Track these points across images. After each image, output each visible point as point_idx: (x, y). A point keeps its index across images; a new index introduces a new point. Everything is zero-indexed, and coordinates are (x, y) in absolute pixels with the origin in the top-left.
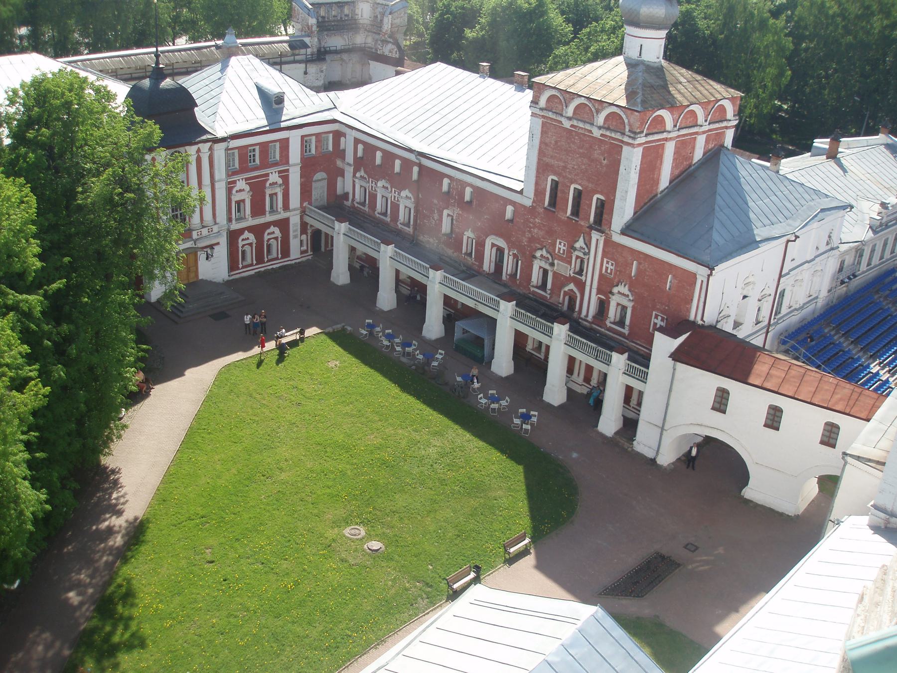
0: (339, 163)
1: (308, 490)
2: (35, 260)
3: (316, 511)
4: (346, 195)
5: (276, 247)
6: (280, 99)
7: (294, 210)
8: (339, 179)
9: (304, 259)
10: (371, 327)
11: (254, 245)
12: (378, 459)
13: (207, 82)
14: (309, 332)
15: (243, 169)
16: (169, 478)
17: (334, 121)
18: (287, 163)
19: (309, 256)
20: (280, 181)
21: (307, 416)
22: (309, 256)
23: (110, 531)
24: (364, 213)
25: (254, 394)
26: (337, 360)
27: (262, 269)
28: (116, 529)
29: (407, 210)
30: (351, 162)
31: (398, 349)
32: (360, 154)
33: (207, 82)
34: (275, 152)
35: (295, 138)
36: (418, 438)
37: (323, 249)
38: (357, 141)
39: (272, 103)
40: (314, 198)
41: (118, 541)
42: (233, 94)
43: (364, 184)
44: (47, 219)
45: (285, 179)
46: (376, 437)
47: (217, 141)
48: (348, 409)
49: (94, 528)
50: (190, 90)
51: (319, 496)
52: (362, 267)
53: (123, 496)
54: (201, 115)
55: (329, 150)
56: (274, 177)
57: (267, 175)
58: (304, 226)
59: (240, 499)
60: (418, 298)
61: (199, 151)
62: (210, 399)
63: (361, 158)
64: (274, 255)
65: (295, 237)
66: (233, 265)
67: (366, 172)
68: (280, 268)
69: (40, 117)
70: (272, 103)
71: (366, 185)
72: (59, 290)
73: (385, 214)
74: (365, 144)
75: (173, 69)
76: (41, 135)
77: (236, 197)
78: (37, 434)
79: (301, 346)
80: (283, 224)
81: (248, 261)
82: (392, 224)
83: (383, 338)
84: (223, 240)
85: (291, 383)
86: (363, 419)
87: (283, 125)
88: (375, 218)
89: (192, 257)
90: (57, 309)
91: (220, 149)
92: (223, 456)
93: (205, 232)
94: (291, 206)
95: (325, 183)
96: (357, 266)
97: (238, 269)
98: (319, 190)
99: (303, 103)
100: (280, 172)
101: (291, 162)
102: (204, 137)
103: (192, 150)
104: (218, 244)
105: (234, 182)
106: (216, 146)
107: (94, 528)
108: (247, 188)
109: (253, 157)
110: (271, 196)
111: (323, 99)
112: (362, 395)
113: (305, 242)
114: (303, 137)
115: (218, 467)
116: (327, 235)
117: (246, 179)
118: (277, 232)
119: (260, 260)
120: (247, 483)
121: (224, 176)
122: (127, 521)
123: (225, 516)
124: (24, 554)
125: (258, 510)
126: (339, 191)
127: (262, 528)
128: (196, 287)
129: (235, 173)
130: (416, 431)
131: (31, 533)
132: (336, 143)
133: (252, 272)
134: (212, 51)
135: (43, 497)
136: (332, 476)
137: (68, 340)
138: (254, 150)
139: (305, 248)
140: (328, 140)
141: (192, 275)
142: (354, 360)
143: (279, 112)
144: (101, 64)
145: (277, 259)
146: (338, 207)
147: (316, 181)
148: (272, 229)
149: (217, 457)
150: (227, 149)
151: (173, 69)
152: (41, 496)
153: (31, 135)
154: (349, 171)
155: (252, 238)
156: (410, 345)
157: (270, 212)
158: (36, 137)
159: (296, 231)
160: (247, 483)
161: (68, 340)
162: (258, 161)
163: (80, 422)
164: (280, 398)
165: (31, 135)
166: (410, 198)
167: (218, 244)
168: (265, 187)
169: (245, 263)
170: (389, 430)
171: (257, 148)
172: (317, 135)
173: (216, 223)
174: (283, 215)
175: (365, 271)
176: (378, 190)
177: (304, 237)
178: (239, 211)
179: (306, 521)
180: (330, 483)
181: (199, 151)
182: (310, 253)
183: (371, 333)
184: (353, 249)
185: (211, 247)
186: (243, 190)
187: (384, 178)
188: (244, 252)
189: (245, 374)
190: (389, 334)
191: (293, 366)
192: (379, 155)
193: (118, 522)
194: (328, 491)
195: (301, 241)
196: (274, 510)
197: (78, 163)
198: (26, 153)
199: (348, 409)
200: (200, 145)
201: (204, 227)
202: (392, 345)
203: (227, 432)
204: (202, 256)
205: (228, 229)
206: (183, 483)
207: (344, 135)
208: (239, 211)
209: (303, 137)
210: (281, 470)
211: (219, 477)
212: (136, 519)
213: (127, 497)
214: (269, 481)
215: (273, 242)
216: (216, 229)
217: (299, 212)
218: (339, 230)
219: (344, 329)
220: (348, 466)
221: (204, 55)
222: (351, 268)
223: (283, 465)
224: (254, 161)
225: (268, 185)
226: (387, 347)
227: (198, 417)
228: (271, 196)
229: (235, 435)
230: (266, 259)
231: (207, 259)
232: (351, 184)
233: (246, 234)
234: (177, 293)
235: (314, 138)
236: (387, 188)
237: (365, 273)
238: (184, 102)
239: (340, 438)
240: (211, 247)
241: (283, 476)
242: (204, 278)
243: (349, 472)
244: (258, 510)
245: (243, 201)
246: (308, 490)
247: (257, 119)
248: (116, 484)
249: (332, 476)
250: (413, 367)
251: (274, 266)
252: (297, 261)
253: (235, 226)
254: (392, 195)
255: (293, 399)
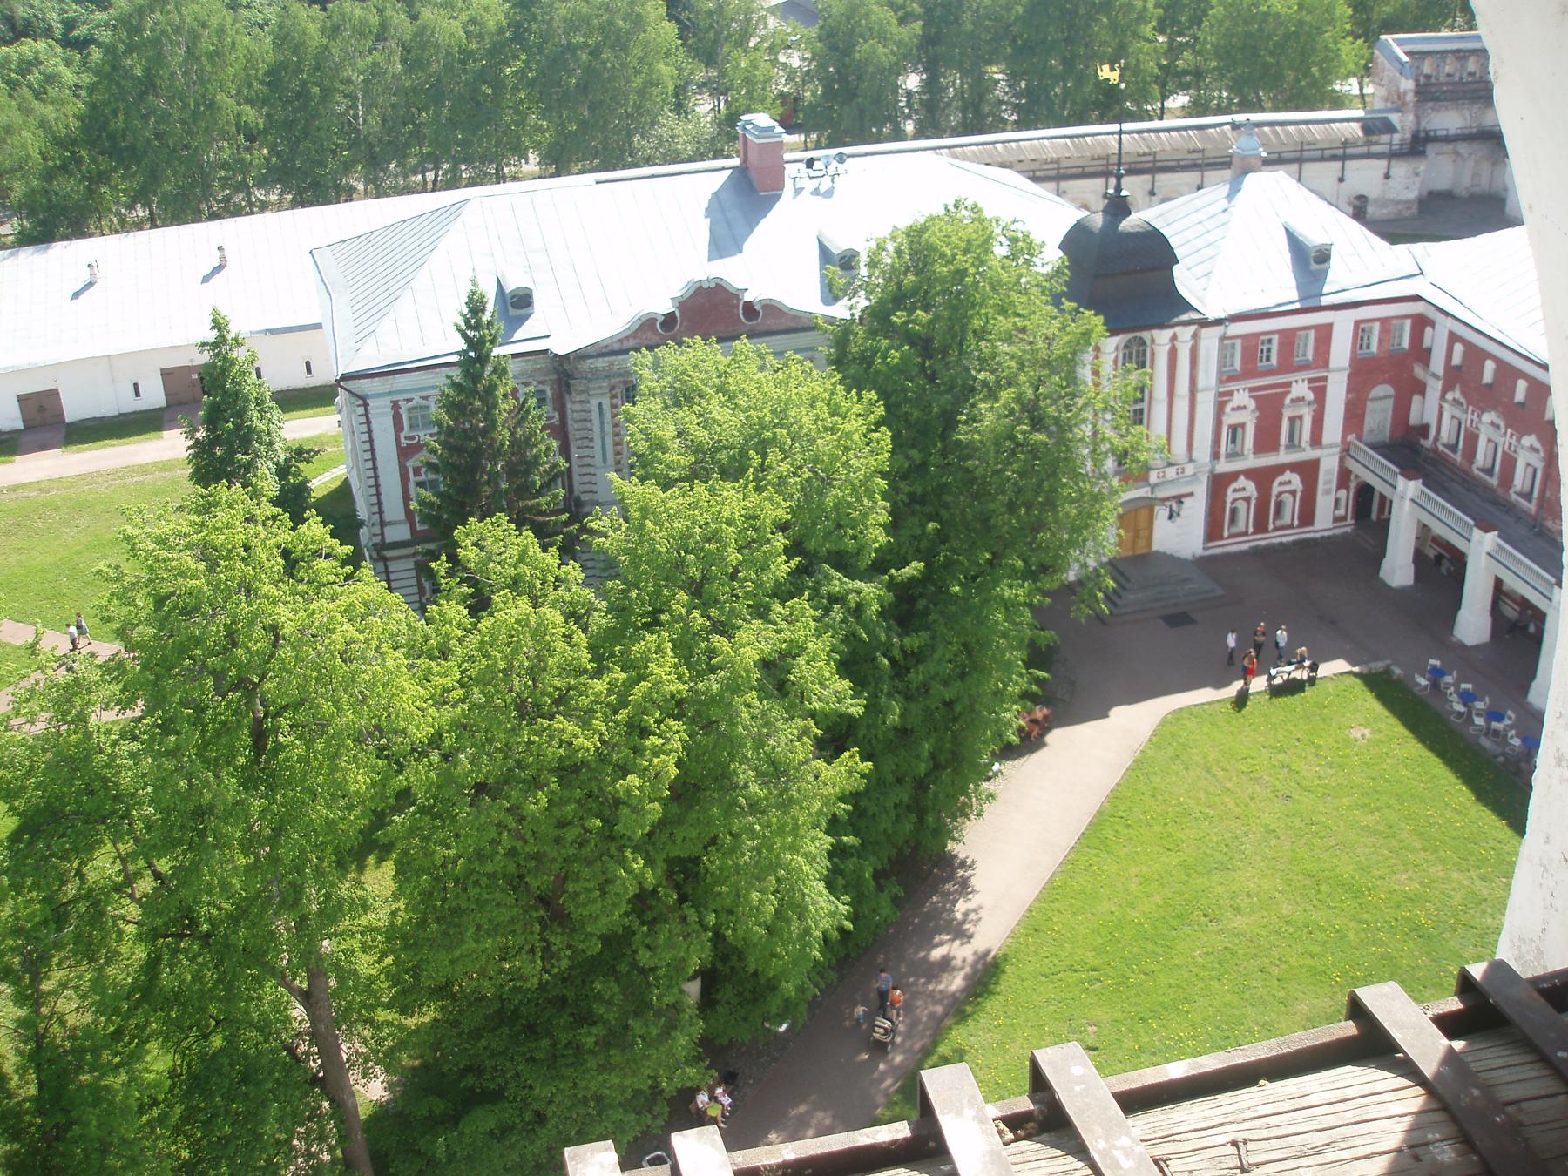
0: (1418, 371)
1: (1275, 953)
2: (878, 531)
3: (1282, 994)
4: (1424, 430)
5: (1291, 508)
6: (1323, 256)
7: (1331, 446)
8: (1416, 399)
9: (1338, 531)
10: (1437, 674)
11: (1253, 502)
12: (1407, 920)
13: (1200, 216)
14: (1325, 669)
15: (1249, 371)
16: (1051, 892)
17: (1417, 298)
18: (1326, 365)
19: (1347, 527)
20: (1310, 396)
21: (1297, 823)
22: (1347, 527)
23: (946, 964)
24: (1451, 465)
25: (1215, 769)
26: (1369, 726)
27: (1263, 543)
28: (958, 962)
29: (1530, 470)
30: (1440, 372)
31: (1479, 721)
32: (1457, 359)
33: (1200, 216)
34: (1306, 345)
35: (1343, 326)
36: (1485, 892)
37: (1374, 516)
38: (1453, 338)
39: (1310, 261)
40: (1366, 428)
41: (955, 983)
42: (1239, 242)
43: (1458, 413)
44: (907, 457)
45: (1320, 392)
46: (1410, 879)
47: (1205, 323)
48: (1370, 820)
49: (922, 954)
50: (1173, 242)
51: (1292, 968)
52: (1439, 558)
53: (975, 911)
54: (1185, 280)
55: (1403, 352)
56: (1301, 389)
57: (1289, 384)
58: (1344, 476)
59: (1160, 950)
60: (1532, 629)
61: (1174, 338)
62: (1140, 767)
63: (1458, 368)
64: (1287, 519)
65: (1327, 492)
66: (1213, 531)
67: (1464, 393)
68: (1295, 543)
69: (915, 291)
70: (1310, 261)
71: (1463, 417)
72: (912, 579)
73: (1490, 472)
74: (1467, 344)
75: (1155, 161)
76: (914, 322)
77: (1230, 418)
78: (850, 807)
79: (1309, 692)
80: (1309, 471)
81: (1241, 526)
82: (1500, 491)
83: (1455, 698)
84: (1201, 490)
85: (1281, 757)
86: (1394, 842)
87: (1325, 301)
88: (1473, 477)
89: (1144, 514)
90: (906, 608)
91: (1210, 338)
92: (1144, 869)
93: (1171, 473)
94: (1326, 440)
95: (1390, 404)
96: (1431, 553)
97: (1222, 538)
98: (1379, 415)
99: (1366, 266)
100: (1311, 381)
101: (1332, 365)
102: (1185, 317)
103: (1162, 337)
104: (1191, 494)
105: (1230, 393)
106: (1205, 332)
107: (922, 954)
108: (1252, 404)
109: (1268, 355)
110: (1292, 420)
111: (1404, 255)
112: (1399, 797)
113: (1343, 502)
114: (1357, 323)
115: (1133, 887)
116: (1383, 497)
117: (1252, 390)
118: (1295, 481)
119: (1261, 526)
120: (1174, 923)
121: (1213, 380)
122: (975, 953)
123: (1129, 974)
124: (801, 990)
125: (1186, 975)
126: (1414, 419)
127: (1186, 1007)
128: (1138, 565)
129: (1233, 378)
130: (1483, 878)
131: (816, 962)
132: (1417, 335)
133: (1245, 547)
134: (1224, 133)
135: (844, 909)
136: (1321, 937)
137: (917, 657)
138: (1270, 341)
139: (1342, 512)
140: (1402, 329)
141: (1141, 543)
142: (1400, 729)
143: (1320, 278)
144: (1034, 149)
145: (1291, 526)
146: (1408, 449)
147: (1374, 399)
148: (1288, 475)
149: (1134, 871)
150: (1223, 338)
151: (1155, 161)
152: (841, 907)
153: (898, 318)
154: (1434, 388)
155: (1251, 488)
156: (1500, 718)
157: (1287, 447)
158: (906, 323)
159: (1329, 482)
160: (1174, 923)
161: (917, 657)
162: (1274, 361)
163: (921, 786)
164: (1256, 780)
165: (898, 318)
166: (1537, 451)
167: (1191, 494)
168: (1282, 405)
169: (1234, 530)
170: (1437, 871)
171: (1275, 338)
172: (1384, 321)
173: (1191, 460)
174: (1308, 454)
175: (1442, 568)
176: (1482, 428)
177: (1343, 493)
178: (1234, 441)
179: (1261, 1009)
180: (1315, 949)
181: (1174, 338)
182: (1350, 521)
183: (1435, 685)
184: (1424, 529)
185: (1179, 499)
186: (1244, 408)
187: (1494, 408)
188: (1234, 512)
189: (1205, 730)
190: (1466, 691)
191: (1289, 726)
192: (1489, 366)
193: (962, 953)
194: (1310, 962)
195: (1337, 501)
196: (1212, 979)
197: (967, 370)
198: (888, 349)
199: (1370, 820)
200: (1177, 329)
201: (1170, 464)
202: (1470, 712)
203: (1157, 829)
204: (1161, 514)
205: (1212, 472)
206: (1071, 905)
207: (1432, 324)
208: (1234, 441)
209: (1357, 323)
210: (1237, 910)
211: (1132, 905)
212: (988, 952)
213: (982, 913)
214: (1213, 927)
215: (1288, 498)
216: (1190, 469)
217: (1336, 450)
218: (1405, 491)
219: (1387, 671)
220: (1352, 924)
221: (1210, 139)
222: (1419, 557)
223: (1242, 902)
224: (1268, 359)
225: (1287, 401)
226: (1460, 714)
227: (1115, 796)
228: (1292, 420)
229: (1170, 835)
230: (1271, 527)
231: (1170, 517)
232: (1438, 412)
233: (1242, 481)
234: (1100, 595)
235: (1377, 326)
236: (1498, 427)
237: (1444, 570)
238: (1156, 253)
239: (1347, 870)
240: (1179, 499)
241: (1239, 922)
242: (1162, 549)
243: (1351, 935)
244: (1186, 975)
245: (1243, 426)
246: (1275, 953)
247: (1281, 288)
248: (965, 887)
249: (1321, 937)
250: (1501, 759)
251: (1284, 540)
252: (1326, 534)
253: (1224, 467)
254: (1505, 439)
255: (1279, 786)
